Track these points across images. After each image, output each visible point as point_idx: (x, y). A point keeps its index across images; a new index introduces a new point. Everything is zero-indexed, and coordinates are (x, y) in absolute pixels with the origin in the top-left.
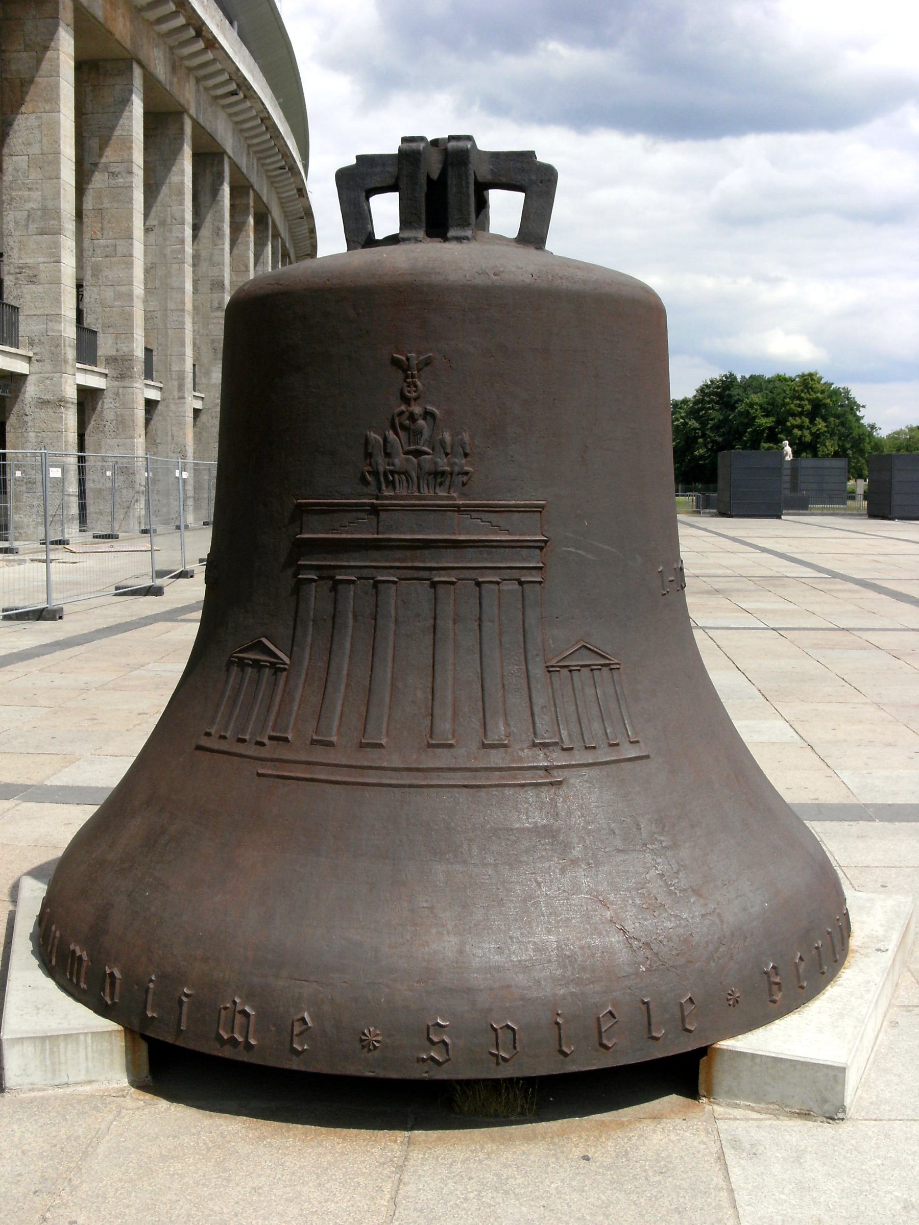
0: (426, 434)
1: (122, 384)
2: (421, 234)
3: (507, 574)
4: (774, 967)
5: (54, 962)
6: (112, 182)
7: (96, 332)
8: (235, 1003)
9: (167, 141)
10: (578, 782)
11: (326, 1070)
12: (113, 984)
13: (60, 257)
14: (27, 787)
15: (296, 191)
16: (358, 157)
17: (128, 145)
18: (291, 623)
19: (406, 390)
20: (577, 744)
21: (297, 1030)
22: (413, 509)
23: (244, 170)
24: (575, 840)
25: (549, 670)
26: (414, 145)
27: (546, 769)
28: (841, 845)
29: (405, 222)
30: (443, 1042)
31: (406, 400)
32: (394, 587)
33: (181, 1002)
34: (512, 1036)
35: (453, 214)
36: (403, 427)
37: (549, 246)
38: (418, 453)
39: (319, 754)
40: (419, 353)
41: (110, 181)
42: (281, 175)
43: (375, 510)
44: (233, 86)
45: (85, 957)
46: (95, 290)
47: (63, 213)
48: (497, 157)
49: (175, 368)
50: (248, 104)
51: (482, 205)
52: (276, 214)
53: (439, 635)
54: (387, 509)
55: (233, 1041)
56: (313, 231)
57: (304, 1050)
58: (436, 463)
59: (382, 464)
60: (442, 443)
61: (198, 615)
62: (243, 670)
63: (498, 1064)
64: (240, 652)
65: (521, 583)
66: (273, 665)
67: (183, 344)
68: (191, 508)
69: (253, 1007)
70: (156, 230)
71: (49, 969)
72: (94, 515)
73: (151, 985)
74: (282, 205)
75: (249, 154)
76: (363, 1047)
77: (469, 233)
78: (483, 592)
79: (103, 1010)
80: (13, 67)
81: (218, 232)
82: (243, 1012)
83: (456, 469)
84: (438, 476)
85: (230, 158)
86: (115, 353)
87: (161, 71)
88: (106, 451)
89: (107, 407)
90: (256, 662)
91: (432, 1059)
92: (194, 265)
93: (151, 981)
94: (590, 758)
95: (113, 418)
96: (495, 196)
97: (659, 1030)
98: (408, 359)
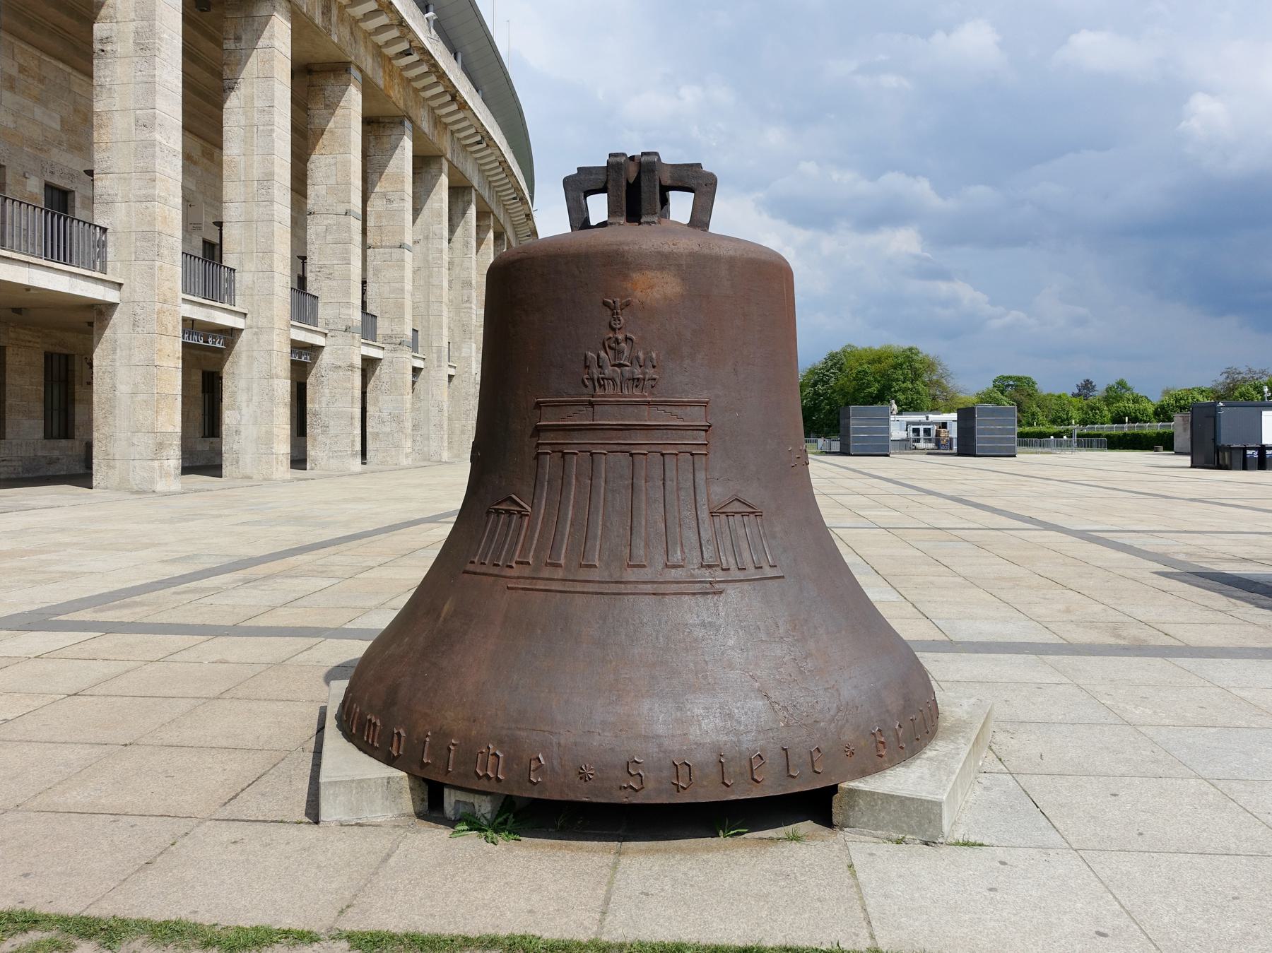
2: (622, 220)
3: (654, 448)
10: (732, 592)
11: (557, 797)
12: (399, 740)
14: (327, 629)
20: (733, 567)
21: (533, 767)
22: (618, 404)
25: (712, 514)
26: (618, 159)
27: (711, 583)
28: (938, 667)
29: (611, 213)
31: (614, 330)
33: (449, 750)
35: (645, 205)
37: (712, 229)
38: (620, 366)
39: (546, 573)
40: (622, 298)
44: (479, 138)
45: (378, 723)
50: (489, 151)
51: (665, 202)
52: (510, 232)
59: (595, 372)
60: (638, 358)
61: (454, 519)
65: (692, 454)
69: (502, 751)
71: (349, 736)
74: (515, 227)
77: (655, 219)
79: (390, 761)
80: (317, 121)
81: (466, 244)
82: (495, 754)
84: (636, 381)
87: (426, 126)
89: (382, 372)
90: (507, 511)
91: (632, 787)
94: (741, 575)
96: (674, 196)
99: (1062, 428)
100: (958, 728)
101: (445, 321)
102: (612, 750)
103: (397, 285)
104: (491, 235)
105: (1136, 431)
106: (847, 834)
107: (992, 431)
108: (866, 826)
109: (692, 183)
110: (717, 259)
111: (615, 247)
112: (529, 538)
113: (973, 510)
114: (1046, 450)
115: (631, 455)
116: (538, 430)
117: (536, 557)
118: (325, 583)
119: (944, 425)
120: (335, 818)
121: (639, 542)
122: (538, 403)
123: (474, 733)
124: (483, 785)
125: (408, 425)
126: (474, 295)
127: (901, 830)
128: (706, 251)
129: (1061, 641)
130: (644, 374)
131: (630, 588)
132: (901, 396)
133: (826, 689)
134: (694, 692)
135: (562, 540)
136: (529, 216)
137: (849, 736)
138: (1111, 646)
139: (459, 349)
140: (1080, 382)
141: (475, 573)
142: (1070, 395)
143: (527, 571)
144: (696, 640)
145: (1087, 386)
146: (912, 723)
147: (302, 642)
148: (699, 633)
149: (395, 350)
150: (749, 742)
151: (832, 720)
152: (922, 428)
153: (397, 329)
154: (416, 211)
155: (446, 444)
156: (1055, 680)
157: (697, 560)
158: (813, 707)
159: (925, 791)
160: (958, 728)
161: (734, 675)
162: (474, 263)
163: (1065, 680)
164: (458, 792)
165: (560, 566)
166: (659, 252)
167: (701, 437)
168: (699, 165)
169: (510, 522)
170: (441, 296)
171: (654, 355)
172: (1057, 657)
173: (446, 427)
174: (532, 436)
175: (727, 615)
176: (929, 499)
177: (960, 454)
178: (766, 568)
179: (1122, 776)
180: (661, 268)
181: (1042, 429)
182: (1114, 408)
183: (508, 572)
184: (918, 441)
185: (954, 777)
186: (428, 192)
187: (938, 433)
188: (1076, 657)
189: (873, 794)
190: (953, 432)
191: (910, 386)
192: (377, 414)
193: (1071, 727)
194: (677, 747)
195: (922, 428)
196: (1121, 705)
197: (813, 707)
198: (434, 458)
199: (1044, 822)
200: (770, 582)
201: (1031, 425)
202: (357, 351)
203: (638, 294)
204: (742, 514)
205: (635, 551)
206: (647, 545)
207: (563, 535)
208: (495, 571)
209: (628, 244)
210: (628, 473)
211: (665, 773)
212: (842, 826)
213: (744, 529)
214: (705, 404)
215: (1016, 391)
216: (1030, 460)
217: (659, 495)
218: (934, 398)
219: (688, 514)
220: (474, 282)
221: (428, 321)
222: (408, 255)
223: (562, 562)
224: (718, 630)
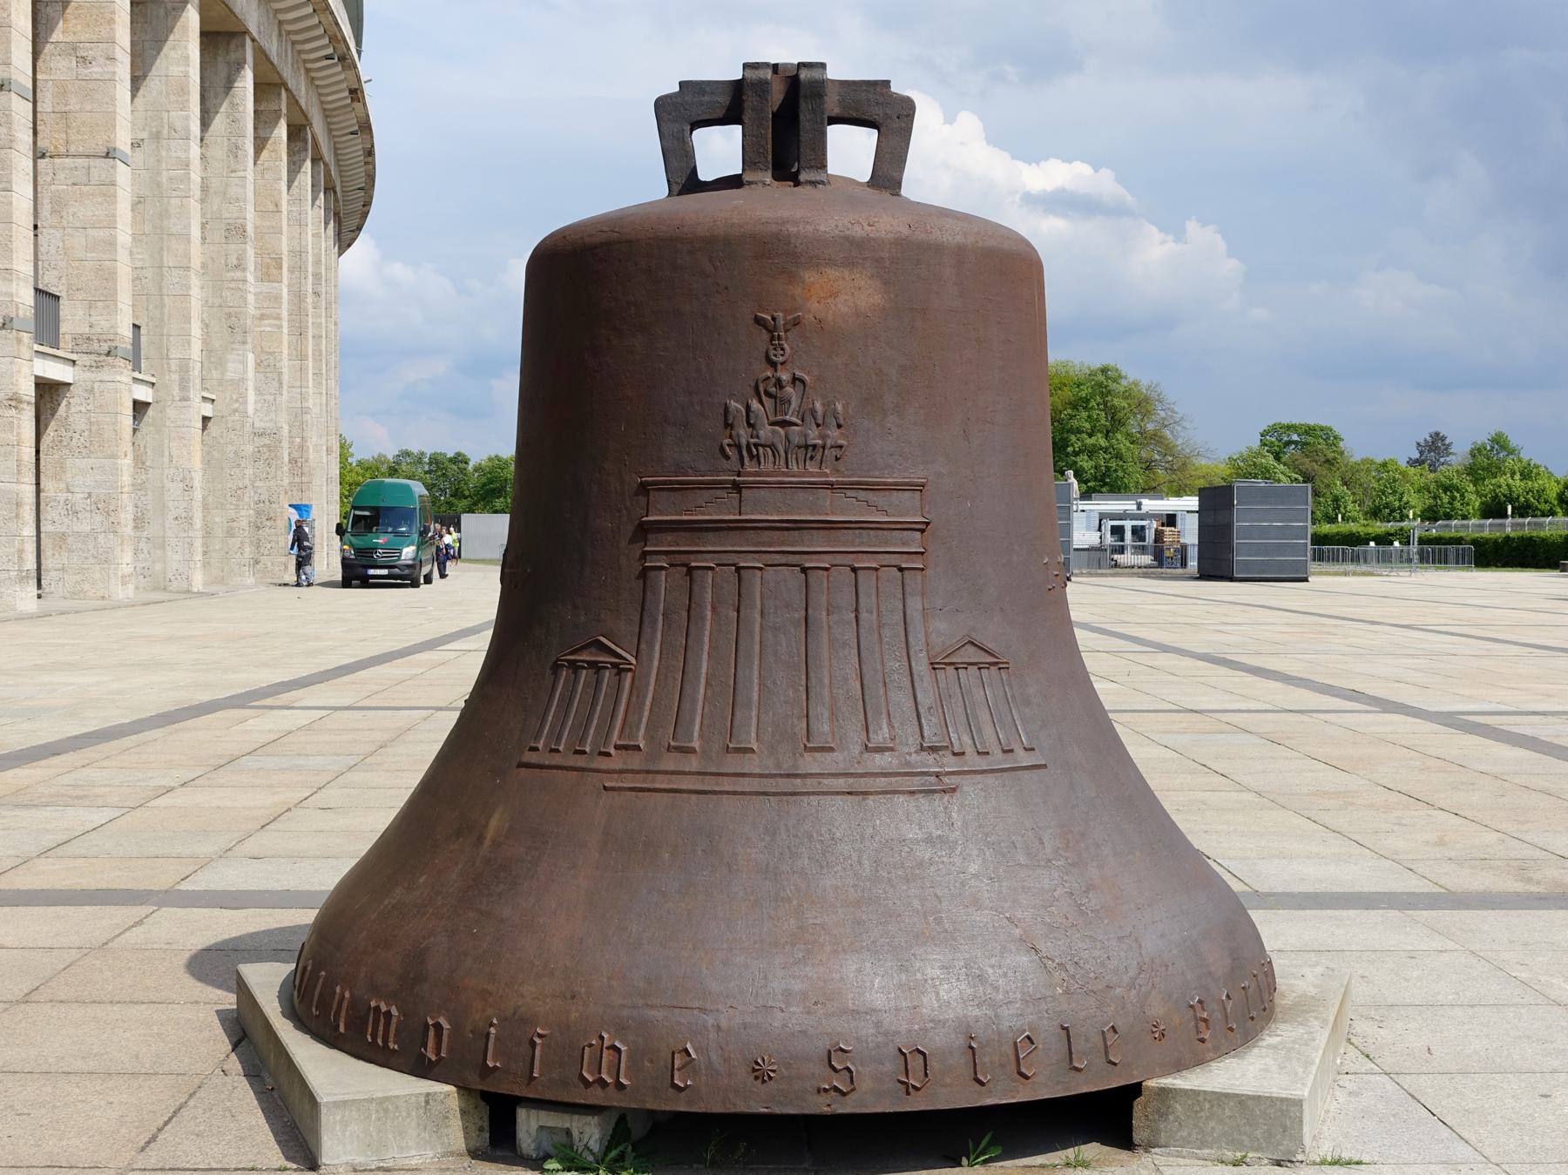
0: (794, 405)
1: (99, 376)
3: (839, 559)
4: (1200, 1002)
5: (342, 1029)
6: (83, 72)
7: (58, 298)
8: (602, 1038)
9: (162, 12)
10: (971, 789)
11: (717, 1108)
13: (10, 182)
15: (346, 93)
16: (681, 83)
17: (108, 16)
18: (637, 619)
19: (772, 352)
20: (969, 750)
21: (677, 1063)
22: (781, 486)
23: (275, 60)
24: (975, 852)
25: (934, 666)
27: (937, 775)
30: (848, 1069)
31: (773, 365)
32: (758, 573)
33: (533, 1044)
34: (921, 1061)
36: (768, 394)
38: (785, 424)
39: (670, 762)
40: (786, 312)
41: (81, 70)
42: (328, 67)
43: (737, 487)
46: (58, 234)
47: (15, 117)
48: (850, 87)
49: (175, 354)
52: (318, 126)
53: (811, 628)
54: (752, 486)
55: (602, 1083)
56: (370, 153)
57: (687, 1086)
58: (806, 436)
60: (813, 412)
62: (575, 672)
63: (908, 1093)
64: (571, 653)
65: (901, 569)
66: (614, 665)
67: (187, 319)
68: (199, 565)
69: (622, 1041)
70: (145, 146)
72: (53, 574)
73: (492, 1030)
74: (327, 114)
75: (280, 35)
76: (756, 1078)
78: (860, 580)
79: (422, 1069)
81: (235, 151)
82: (613, 1047)
83: (829, 442)
85: (253, 40)
86: (87, 330)
88: (74, 476)
89: (71, 409)
91: (836, 1089)
92: (203, 201)
93: (491, 1025)
94: (982, 764)
95: (84, 427)
97: (1081, 1060)
98: (774, 319)
99: (1391, 526)
100: (1304, 1008)
101: (196, 305)
102: (804, 1033)
103: (101, 234)
104: (281, 131)
105: (1527, 532)
106: (1158, 1156)
107: (1264, 533)
108: (1186, 1142)
109: (876, 113)
110: (938, 249)
111: (774, 228)
112: (634, 707)
113: (1250, 678)
114: (1364, 568)
115: (804, 570)
116: (644, 531)
117: (650, 738)
118: (99, 817)
119: (1171, 520)
120: (344, 1159)
121: (821, 713)
122: (643, 485)
123: (574, 1015)
124: (596, 1096)
125: (127, 517)
126: (250, 252)
127: (1239, 1145)
128: (920, 236)
129: (1437, 889)
130: (824, 437)
131: (811, 784)
132: (1085, 462)
133: (1120, 939)
134: (924, 943)
135: (694, 710)
136: (356, 93)
137: (1156, 1009)
138: (1518, 894)
139: (221, 363)
140: (1424, 436)
141: (541, 767)
142: (1403, 464)
143: (635, 761)
144: (920, 865)
145: (1436, 446)
146: (1241, 1000)
147: (120, 915)
148: (925, 853)
149: (98, 366)
150: (1012, 1018)
151: (1132, 986)
152: (1128, 525)
153: (102, 324)
154: (137, 81)
155: (198, 557)
156: (1437, 944)
157: (913, 741)
158: (1103, 965)
159: (1276, 1086)
160: (1304, 1008)
161: (983, 917)
162: (250, 188)
163: (1451, 945)
164: (543, 1114)
165: (692, 751)
166: (847, 238)
167: (914, 542)
168: (887, 83)
169: (598, 682)
170: (187, 255)
171: (839, 407)
172: (1433, 913)
173: (198, 523)
174: (632, 541)
175: (965, 825)
176: (1163, 660)
177: (1205, 575)
178: (1019, 752)
179: (1554, 1072)
180: (849, 264)
181: (1353, 527)
182: (1489, 485)
183: (603, 763)
184: (1121, 550)
185: (1314, 1069)
186: (159, 42)
187: (1159, 536)
188: (1465, 913)
189: (1196, 1093)
190: (1189, 533)
191: (1103, 443)
192: (62, 497)
193: (1470, 1011)
194: (904, 1027)
195: (1128, 525)
196: (1543, 978)
197: (1103, 965)
198: (175, 585)
199: (1446, 1133)
200: (1026, 774)
201: (1333, 520)
202: (25, 369)
203: (814, 306)
204: (980, 666)
205: (814, 725)
206: (833, 715)
207: (694, 701)
208: (580, 761)
209: (796, 223)
210: (798, 599)
211: (888, 1067)
212: (1149, 1146)
213: (984, 689)
214: (920, 488)
215: (1303, 451)
216: (1333, 587)
217: (850, 635)
218: (1149, 466)
219: (895, 665)
220: (250, 228)
221: (162, 306)
222: (123, 173)
223: (696, 744)
224: (952, 849)
